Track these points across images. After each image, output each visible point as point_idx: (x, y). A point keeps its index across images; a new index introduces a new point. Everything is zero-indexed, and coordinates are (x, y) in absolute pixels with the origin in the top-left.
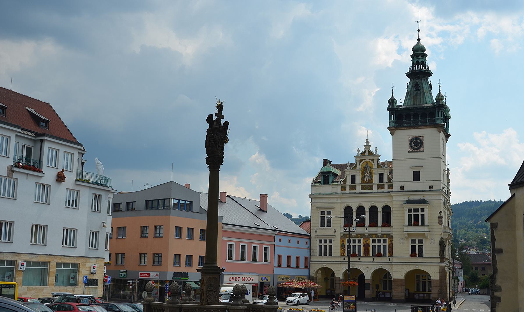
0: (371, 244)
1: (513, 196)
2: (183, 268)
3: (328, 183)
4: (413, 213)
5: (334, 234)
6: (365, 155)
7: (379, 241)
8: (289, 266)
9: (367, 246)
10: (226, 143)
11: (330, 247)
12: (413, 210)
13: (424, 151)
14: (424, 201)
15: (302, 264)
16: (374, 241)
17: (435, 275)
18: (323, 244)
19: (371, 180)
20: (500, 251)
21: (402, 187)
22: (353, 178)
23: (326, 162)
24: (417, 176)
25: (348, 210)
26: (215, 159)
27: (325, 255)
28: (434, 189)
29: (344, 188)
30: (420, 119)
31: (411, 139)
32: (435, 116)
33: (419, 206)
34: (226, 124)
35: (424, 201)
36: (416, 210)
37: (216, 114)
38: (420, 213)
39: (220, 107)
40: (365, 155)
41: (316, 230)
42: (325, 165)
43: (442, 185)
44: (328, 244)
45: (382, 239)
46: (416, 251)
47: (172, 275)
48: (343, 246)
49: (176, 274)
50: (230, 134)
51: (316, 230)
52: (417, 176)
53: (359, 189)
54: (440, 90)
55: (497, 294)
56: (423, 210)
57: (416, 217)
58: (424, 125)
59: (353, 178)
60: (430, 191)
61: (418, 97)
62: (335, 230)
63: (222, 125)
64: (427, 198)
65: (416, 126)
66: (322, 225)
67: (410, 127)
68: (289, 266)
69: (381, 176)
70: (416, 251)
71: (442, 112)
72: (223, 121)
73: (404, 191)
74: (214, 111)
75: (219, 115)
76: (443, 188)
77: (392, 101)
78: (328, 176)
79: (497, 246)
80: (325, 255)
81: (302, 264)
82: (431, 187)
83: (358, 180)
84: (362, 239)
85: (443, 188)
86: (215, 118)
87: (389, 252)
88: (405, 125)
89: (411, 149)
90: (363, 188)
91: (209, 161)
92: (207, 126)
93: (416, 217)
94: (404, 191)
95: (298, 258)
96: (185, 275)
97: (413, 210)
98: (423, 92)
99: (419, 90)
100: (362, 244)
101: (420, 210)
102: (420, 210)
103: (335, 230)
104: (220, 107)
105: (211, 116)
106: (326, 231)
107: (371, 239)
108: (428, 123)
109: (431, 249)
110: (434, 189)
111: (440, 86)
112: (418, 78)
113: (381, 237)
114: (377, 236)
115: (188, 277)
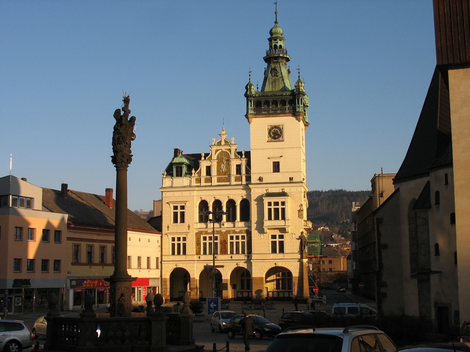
0: (229, 241)
1: (397, 191)
2: (24, 275)
3: (181, 175)
4: (273, 207)
5: (188, 231)
6: (221, 145)
7: (237, 238)
8: (148, 267)
9: (224, 243)
10: (133, 140)
11: (184, 245)
12: (272, 204)
13: (283, 141)
14: (283, 194)
15: (153, 264)
16: (232, 238)
17: (295, 274)
18: (176, 242)
19: (228, 172)
20: (386, 247)
21: (261, 179)
22: (209, 169)
23: (177, 152)
24: (276, 167)
25: (203, 205)
26: (121, 158)
27: (179, 253)
28: (294, 180)
29: (199, 181)
30: (279, 107)
31: (269, 127)
32: (295, 104)
33: (280, 199)
34: (133, 119)
35: (283, 194)
36: (276, 204)
37: (123, 109)
38: (280, 207)
39: (126, 101)
40: (221, 145)
41: (168, 227)
42: (176, 155)
43: (303, 177)
44: (182, 242)
45: (240, 235)
46: (278, 247)
47: (12, 283)
48: (198, 244)
49: (16, 282)
50: (136, 129)
51: (168, 227)
52: (276, 167)
53: (215, 181)
54: (299, 77)
55: (383, 290)
56: (283, 203)
57: (277, 210)
58: (283, 113)
59: (209, 169)
60: (291, 183)
61: (277, 83)
62: (189, 227)
63: (129, 119)
64: (286, 190)
65: (275, 114)
66: (175, 221)
67: (268, 115)
68: (148, 267)
69: (239, 167)
70: (278, 247)
71: (301, 99)
72: (130, 116)
73: (264, 184)
74: (120, 105)
75: (126, 109)
76: (304, 179)
77: (248, 87)
78: (181, 168)
79: (383, 241)
80: (179, 253)
81: (153, 264)
82: (291, 179)
83: (214, 171)
84: (218, 235)
85: (304, 179)
86: (122, 113)
87: (248, 249)
88: (264, 113)
89: (270, 139)
90: (219, 180)
91: (114, 160)
92: (114, 122)
93: (277, 210)
94: (264, 184)
95: (139, 258)
96: (27, 282)
97: (272, 204)
98: (282, 77)
99: (277, 76)
100: (218, 241)
101: (280, 204)
102: (280, 204)
103: (189, 227)
104: (126, 101)
105: (118, 112)
106: (180, 228)
107: (229, 236)
108: (287, 111)
109: (292, 245)
110: (294, 180)
111: (299, 73)
112: (277, 62)
113: (239, 233)
114: (234, 232)
115: (30, 284)
